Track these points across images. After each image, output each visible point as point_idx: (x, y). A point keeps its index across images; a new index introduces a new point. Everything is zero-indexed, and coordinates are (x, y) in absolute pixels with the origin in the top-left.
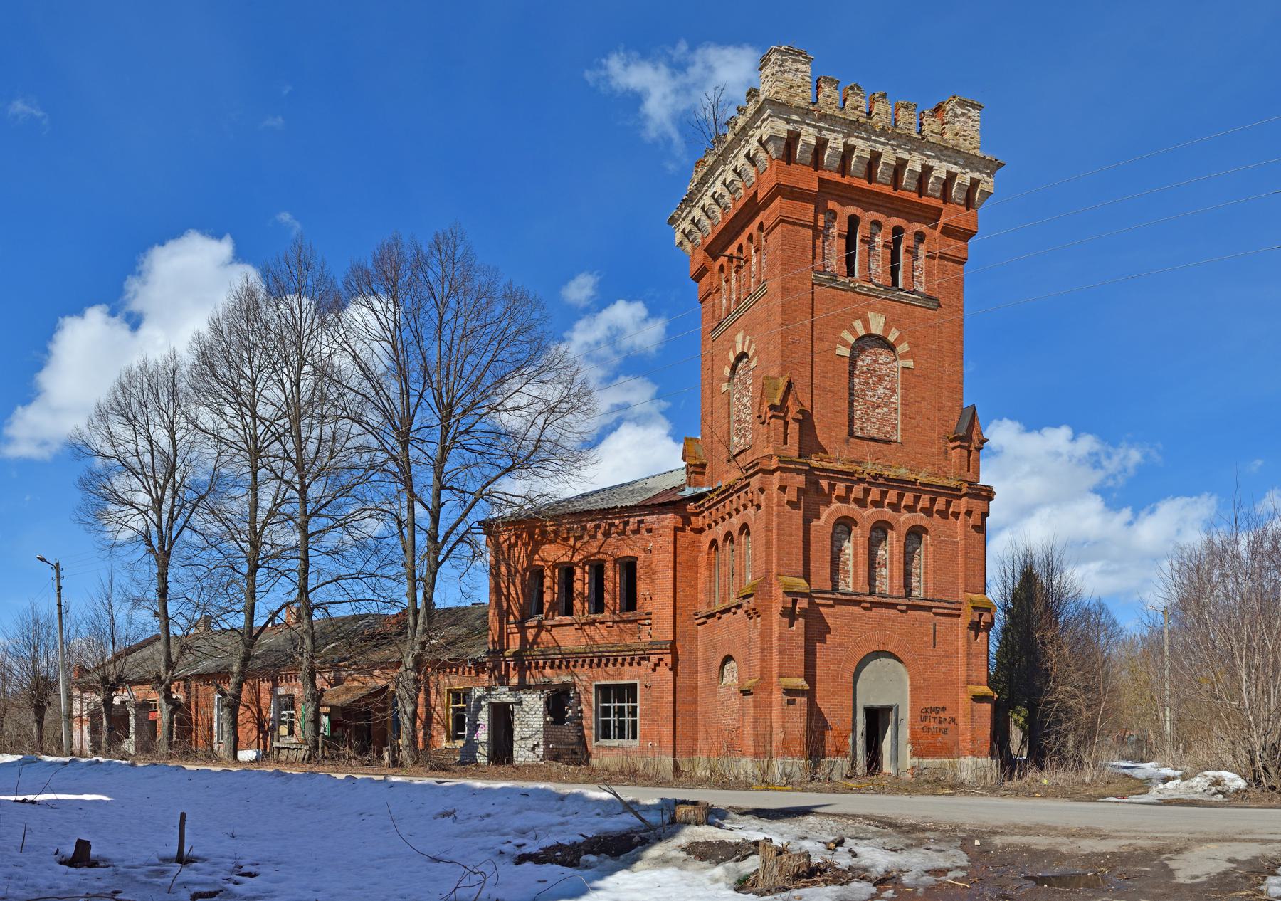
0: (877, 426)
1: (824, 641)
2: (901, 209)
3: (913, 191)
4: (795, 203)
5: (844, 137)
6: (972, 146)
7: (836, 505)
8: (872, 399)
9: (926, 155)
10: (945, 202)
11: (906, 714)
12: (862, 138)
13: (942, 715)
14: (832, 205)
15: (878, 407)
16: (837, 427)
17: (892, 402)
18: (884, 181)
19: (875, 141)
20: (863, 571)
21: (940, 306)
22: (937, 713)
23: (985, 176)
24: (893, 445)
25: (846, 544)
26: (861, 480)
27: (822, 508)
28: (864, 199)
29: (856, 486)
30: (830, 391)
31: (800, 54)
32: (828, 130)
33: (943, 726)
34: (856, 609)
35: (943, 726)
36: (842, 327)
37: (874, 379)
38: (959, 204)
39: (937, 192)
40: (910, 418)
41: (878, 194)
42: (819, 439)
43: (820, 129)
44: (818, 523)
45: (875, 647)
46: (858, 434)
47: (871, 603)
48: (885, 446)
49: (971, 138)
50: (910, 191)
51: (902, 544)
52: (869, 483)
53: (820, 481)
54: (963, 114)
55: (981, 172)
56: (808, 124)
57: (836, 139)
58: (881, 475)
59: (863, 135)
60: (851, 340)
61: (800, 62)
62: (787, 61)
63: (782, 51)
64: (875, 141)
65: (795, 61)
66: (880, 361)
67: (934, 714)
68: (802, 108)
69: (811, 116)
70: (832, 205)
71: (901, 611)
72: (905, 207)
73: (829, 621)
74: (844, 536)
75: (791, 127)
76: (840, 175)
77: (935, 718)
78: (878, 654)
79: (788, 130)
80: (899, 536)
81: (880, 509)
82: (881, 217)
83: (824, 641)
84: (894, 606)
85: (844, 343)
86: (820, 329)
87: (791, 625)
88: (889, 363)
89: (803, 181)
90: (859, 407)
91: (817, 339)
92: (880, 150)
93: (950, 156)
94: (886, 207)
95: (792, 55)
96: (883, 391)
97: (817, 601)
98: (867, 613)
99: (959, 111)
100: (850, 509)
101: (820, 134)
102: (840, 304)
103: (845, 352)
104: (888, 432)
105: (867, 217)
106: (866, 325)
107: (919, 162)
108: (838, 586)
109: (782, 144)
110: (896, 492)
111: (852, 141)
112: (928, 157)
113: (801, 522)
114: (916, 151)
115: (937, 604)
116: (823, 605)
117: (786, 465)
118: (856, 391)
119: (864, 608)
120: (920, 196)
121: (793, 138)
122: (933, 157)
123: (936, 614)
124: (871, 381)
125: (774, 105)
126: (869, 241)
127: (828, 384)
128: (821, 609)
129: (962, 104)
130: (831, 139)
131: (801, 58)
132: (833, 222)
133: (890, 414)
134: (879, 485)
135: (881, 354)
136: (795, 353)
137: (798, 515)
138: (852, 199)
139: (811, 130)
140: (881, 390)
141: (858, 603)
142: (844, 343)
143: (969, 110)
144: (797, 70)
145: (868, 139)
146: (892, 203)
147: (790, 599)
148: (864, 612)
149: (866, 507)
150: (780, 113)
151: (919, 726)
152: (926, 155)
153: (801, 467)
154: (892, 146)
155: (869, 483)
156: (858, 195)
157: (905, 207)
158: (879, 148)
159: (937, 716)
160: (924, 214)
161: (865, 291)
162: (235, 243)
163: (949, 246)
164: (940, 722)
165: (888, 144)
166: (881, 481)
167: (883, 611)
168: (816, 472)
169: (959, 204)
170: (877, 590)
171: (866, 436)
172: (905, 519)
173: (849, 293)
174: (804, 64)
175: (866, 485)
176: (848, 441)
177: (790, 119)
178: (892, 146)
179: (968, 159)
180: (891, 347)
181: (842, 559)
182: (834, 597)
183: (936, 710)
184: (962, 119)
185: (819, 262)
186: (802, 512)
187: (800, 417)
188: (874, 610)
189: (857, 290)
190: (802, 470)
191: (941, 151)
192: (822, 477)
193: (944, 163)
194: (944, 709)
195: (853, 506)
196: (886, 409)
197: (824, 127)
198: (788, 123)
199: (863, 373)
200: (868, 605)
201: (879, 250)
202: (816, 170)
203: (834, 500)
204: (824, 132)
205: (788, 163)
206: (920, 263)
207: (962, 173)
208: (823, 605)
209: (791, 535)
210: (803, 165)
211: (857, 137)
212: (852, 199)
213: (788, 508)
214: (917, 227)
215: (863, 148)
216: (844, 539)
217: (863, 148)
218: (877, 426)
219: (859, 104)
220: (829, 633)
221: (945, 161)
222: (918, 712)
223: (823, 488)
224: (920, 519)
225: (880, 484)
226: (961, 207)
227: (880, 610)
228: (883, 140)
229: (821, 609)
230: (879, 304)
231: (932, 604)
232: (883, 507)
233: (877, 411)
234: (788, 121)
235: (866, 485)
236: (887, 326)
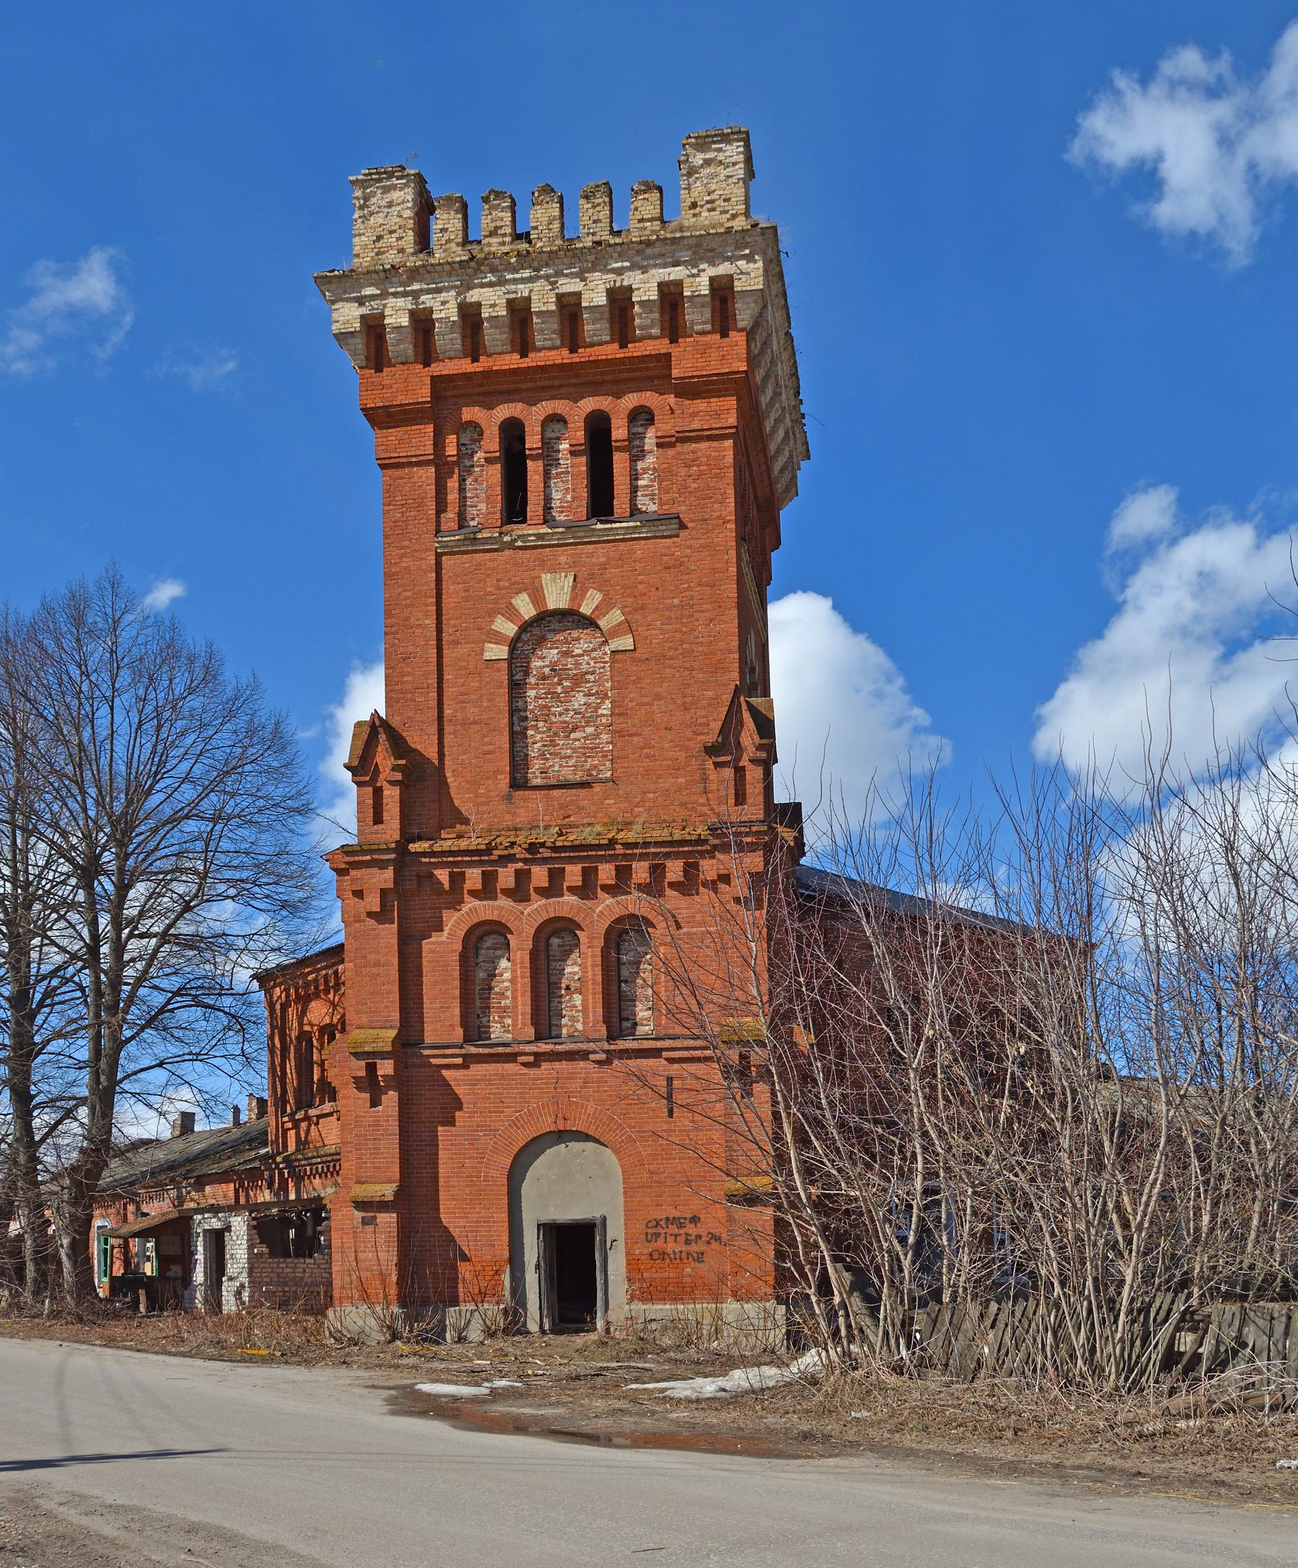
0: (572, 762)
1: (451, 1122)
2: (599, 378)
3: (607, 343)
4: (399, 432)
5: (459, 294)
6: (728, 216)
7: (471, 904)
8: (564, 718)
9: (614, 271)
10: (674, 340)
11: (616, 1230)
12: (491, 285)
13: (691, 1229)
14: (468, 414)
15: (574, 729)
16: (488, 778)
17: (603, 715)
18: (548, 344)
19: (515, 281)
20: (525, 1006)
21: (683, 526)
22: (681, 1226)
23: (742, 263)
24: (597, 788)
25: (504, 963)
26: (507, 859)
27: (445, 914)
28: (524, 386)
29: (500, 870)
30: (475, 723)
31: (390, 175)
32: (429, 292)
33: (695, 1248)
34: (510, 1067)
35: (695, 1248)
36: (493, 614)
37: (566, 684)
38: (703, 333)
39: (651, 327)
40: (631, 735)
41: (544, 369)
42: (457, 803)
43: (415, 295)
44: (440, 939)
45: (547, 1124)
46: (537, 781)
47: (536, 1054)
48: (582, 793)
49: (725, 200)
50: (601, 344)
51: (598, 951)
52: (525, 861)
53: (436, 872)
54: (708, 163)
55: (731, 259)
56: (395, 295)
57: (444, 303)
58: (543, 845)
59: (491, 278)
60: (510, 629)
61: (394, 187)
62: (373, 194)
63: (363, 181)
64: (515, 281)
65: (386, 190)
66: (578, 651)
67: (673, 1229)
68: (376, 272)
69: (394, 280)
70: (468, 414)
71: (600, 1063)
72: (603, 373)
73: (460, 1091)
74: (498, 952)
75: (364, 310)
76: (469, 360)
77: (676, 1236)
78: (561, 1136)
79: (362, 317)
80: (591, 938)
81: (491, 903)
82: (560, 406)
83: (451, 1122)
84: (584, 1055)
85: (497, 638)
86: (454, 626)
87: (375, 1102)
88: (594, 650)
89: (406, 391)
90: (538, 737)
91: (449, 643)
92: (526, 294)
93: (663, 255)
94: (573, 385)
95: (380, 180)
96: (583, 700)
97: (434, 1061)
98: (532, 1072)
99: (698, 159)
100: (501, 908)
101: (417, 304)
102: (489, 576)
103: (498, 652)
104: (596, 767)
105: (533, 416)
106: (537, 596)
107: (602, 288)
108: (489, 1032)
109: (359, 343)
110: (645, 865)
111: (474, 296)
112: (619, 272)
113: (395, 941)
114: (593, 270)
115: (667, 1044)
116: (448, 1067)
117: (356, 858)
118: (532, 711)
119: (524, 1064)
120: (623, 346)
121: (374, 327)
122: (630, 269)
123: (671, 1061)
124: (559, 689)
125: (330, 282)
126: (548, 454)
127: (472, 712)
128: (445, 1073)
129: (703, 144)
130: (436, 306)
131: (394, 181)
132: (479, 441)
133: (597, 736)
134: (545, 861)
135: (578, 639)
136: (409, 674)
137: (389, 933)
138: (502, 392)
139: (400, 302)
140: (579, 700)
141: (511, 1058)
142: (497, 638)
143: (720, 150)
144: (390, 205)
145: (502, 282)
146: (578, 376)
147: (363, 1063)
148: (525, 1070)
149: (529, 900)
150: (345, 292)
151: (642, 1250)
152: (614, 271)
153: (383, 857)
154: (547, 277)
155: (525, 861)
156: (514, 382)
157: (603, 373)
158: (523, 290)
159: (682, 1231)
160: (645, 373)
161: (532, 541)
162: (1116, 505)
163: (694, 415)
164: (687, 1242)
165: (539, 277)
166: (545, 853)
167: (564, 1065)
168: (424, 860)
169: (703, 333)
170: (564, 1031)
171: (553, 782)
172: (606, 908)
173: (507, 552)
174: (401, 189)
175: (520, 865)
176: (509, 797)
177: (363, 297)
178: (547, 277)
179: (698, 245)
180: (589, 623)
181: (497, 989)
182: (463, 1051)
183: (679, 1222)
184: (707, 171)
185: (451, 515)
186: (395, 925)
187: (398, 776)
188: (545, 1066)
189: (519, 543)
190: (388, 860)
191: (639, 252)
192: (437, 865)
193: (653, 271)
194: (695, 1220)
195: (503, 902)
196: (590, 730)
197: (421, 290)
198: (361, 304)
199: (544, 678)
200: (531, 1059)
201: (565, 461)
202: (427, 364)
203: (466, 897)
204: (423, 298)
205: (379, 369)
206: (650, 460)
207: (693, 276)
208: (448, 1067)
209: (377, 964)
210: (403, 364)
211: (482, 286)
212: (502, 392)
213: (371, 922)
214: (631, 400)
215: (491, 300)
216: (499, 957)
217: (491, 300)
218: (572, 762)
219: (499, 224)
220: (461, 1109)
221: (655, 266)
222: (640, 1227)
223: (440, 883)
224: (635, 903)
225: (544, 859)
226: (708, 338)
227: (557, 1065)
228: (526, 273)
229: (445, 1073)
230: (563, 557)
231: (659, 1044)
232: (562, 895)
233: (572, 736)
234: (361, 301)
235: (520, 865)
236: (578, 591)
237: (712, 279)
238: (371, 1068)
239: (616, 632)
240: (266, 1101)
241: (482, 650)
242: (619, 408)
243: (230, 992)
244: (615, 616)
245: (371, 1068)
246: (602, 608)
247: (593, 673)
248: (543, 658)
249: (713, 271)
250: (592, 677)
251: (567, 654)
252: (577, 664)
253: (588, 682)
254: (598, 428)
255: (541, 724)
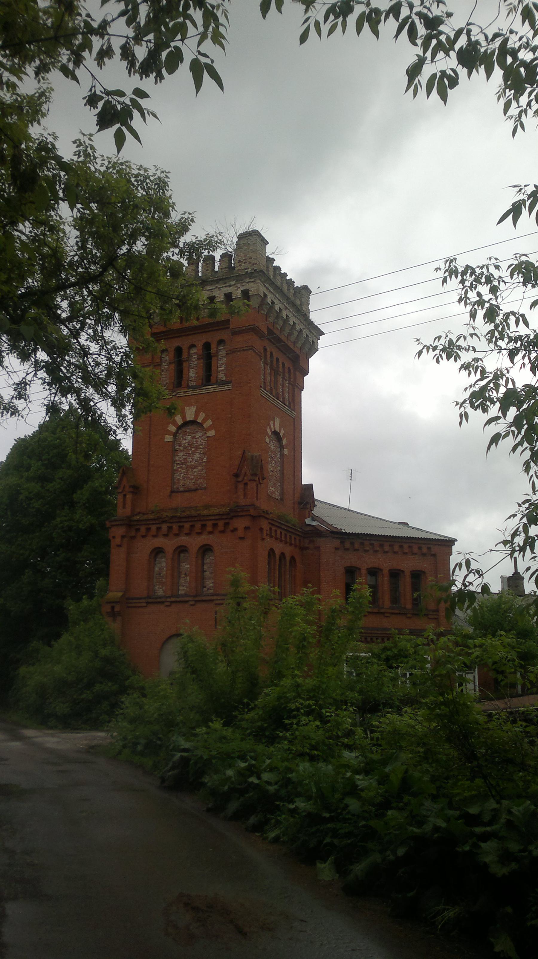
37: (193, 449)
66: (197, 436)
90: (183, 471)
96: (198, 456)
124: (190, 452)
237: (242, 291)
238: (113, 608)
239: (210, 428)
240: (289, 748)
241: (164, 438)
242: (213, 338)
243: (362, 635)
244: (209, 423)
245: (113, 608)
246: (205, 420)
247: (202, 445)
248: (185, 440)
249: (242, 288)
250: (201, 447)
251: (193, 438)
252: (197, 442)
253: (200, 448)
254: (207, 346)
255: (184, 466)
